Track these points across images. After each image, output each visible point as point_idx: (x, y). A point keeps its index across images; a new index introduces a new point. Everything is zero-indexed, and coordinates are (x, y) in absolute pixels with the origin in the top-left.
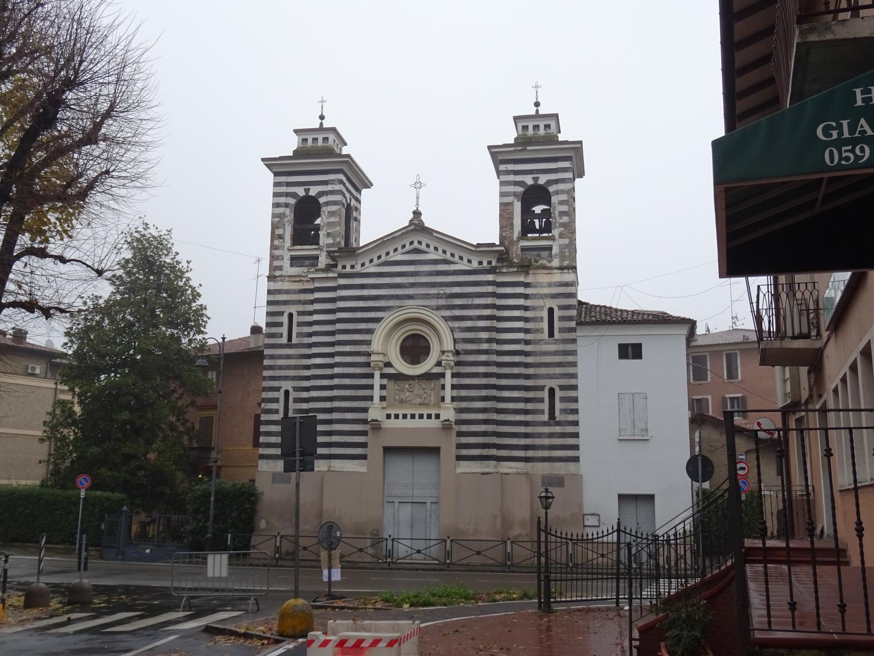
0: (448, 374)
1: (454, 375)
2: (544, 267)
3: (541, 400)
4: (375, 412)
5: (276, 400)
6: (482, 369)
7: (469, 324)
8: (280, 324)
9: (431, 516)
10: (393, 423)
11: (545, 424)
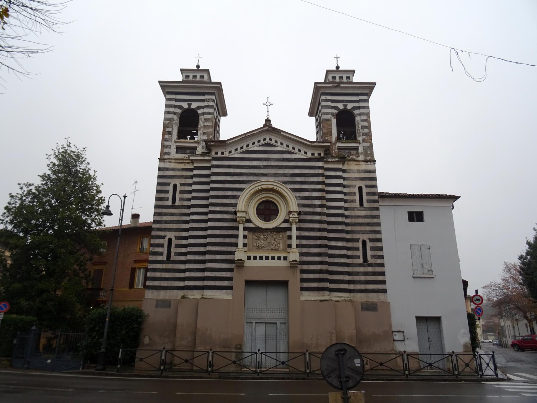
0: (294, 227)
1: (298, 229)
2: (354, 160)
3: (357, 249)
4: (240, 254)
5: (162, 246)
6: (317, 226)
8: (167, 192)
9: (280, 334)
11: (360, 265)
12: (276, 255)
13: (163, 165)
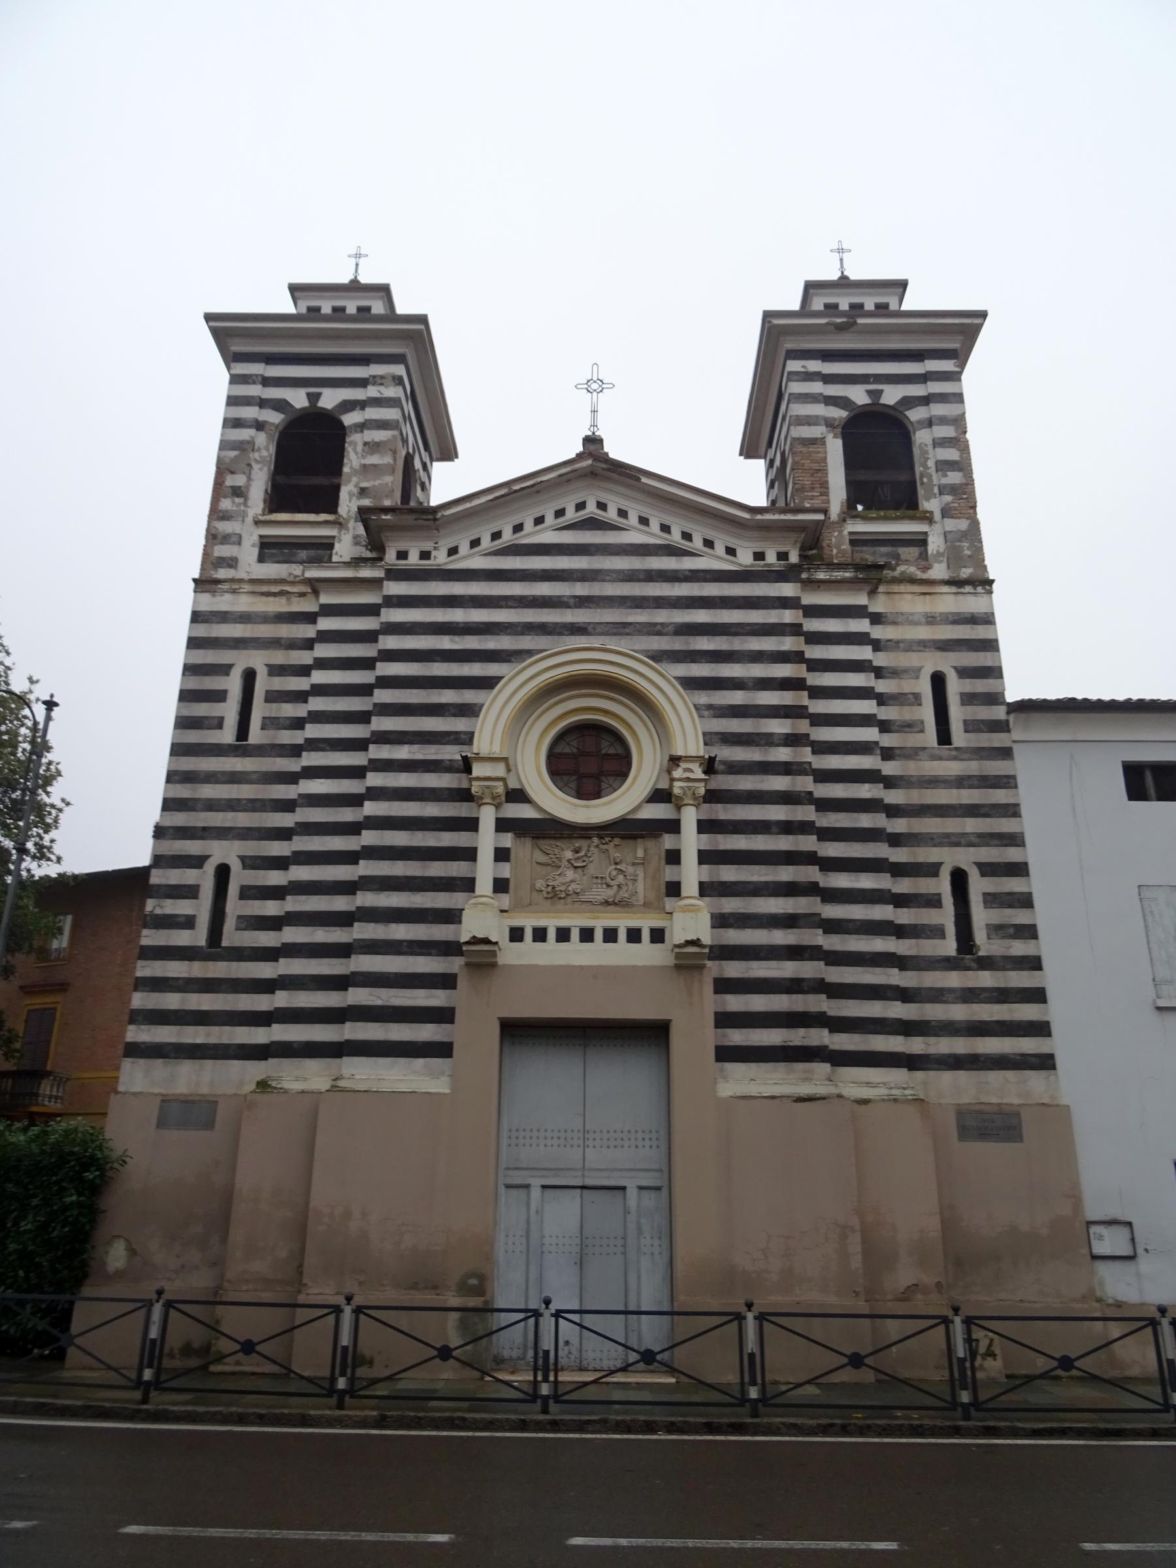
0: (690, 818)
1: (704, 826)
2: (913, 581)
3: (934, 901)
4: (481, 918)
5: (191, 892)
6: (777, 813)
7: (737, 698)
8: (219, 696)
10: (527, 953)
11: (948, 964)
12: (623, 922)
13: (209, 603)
